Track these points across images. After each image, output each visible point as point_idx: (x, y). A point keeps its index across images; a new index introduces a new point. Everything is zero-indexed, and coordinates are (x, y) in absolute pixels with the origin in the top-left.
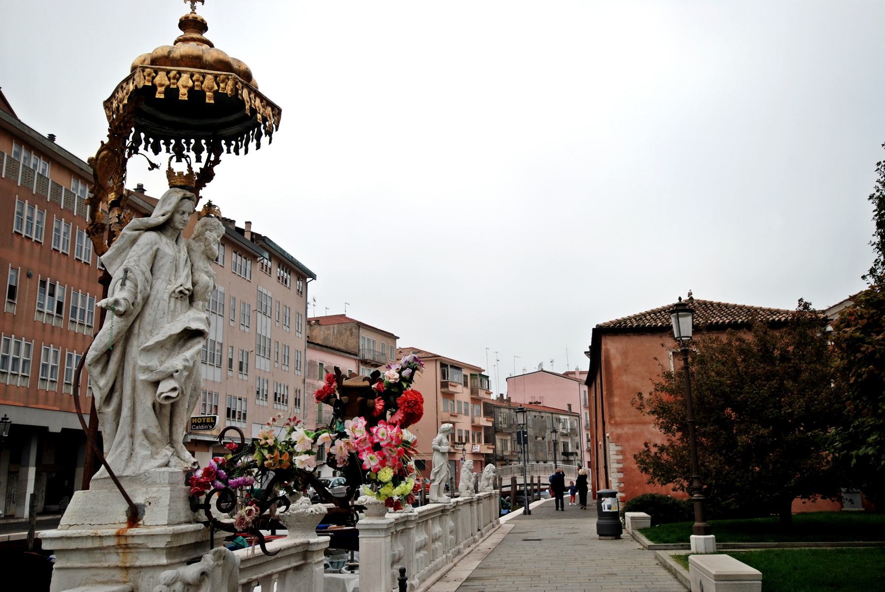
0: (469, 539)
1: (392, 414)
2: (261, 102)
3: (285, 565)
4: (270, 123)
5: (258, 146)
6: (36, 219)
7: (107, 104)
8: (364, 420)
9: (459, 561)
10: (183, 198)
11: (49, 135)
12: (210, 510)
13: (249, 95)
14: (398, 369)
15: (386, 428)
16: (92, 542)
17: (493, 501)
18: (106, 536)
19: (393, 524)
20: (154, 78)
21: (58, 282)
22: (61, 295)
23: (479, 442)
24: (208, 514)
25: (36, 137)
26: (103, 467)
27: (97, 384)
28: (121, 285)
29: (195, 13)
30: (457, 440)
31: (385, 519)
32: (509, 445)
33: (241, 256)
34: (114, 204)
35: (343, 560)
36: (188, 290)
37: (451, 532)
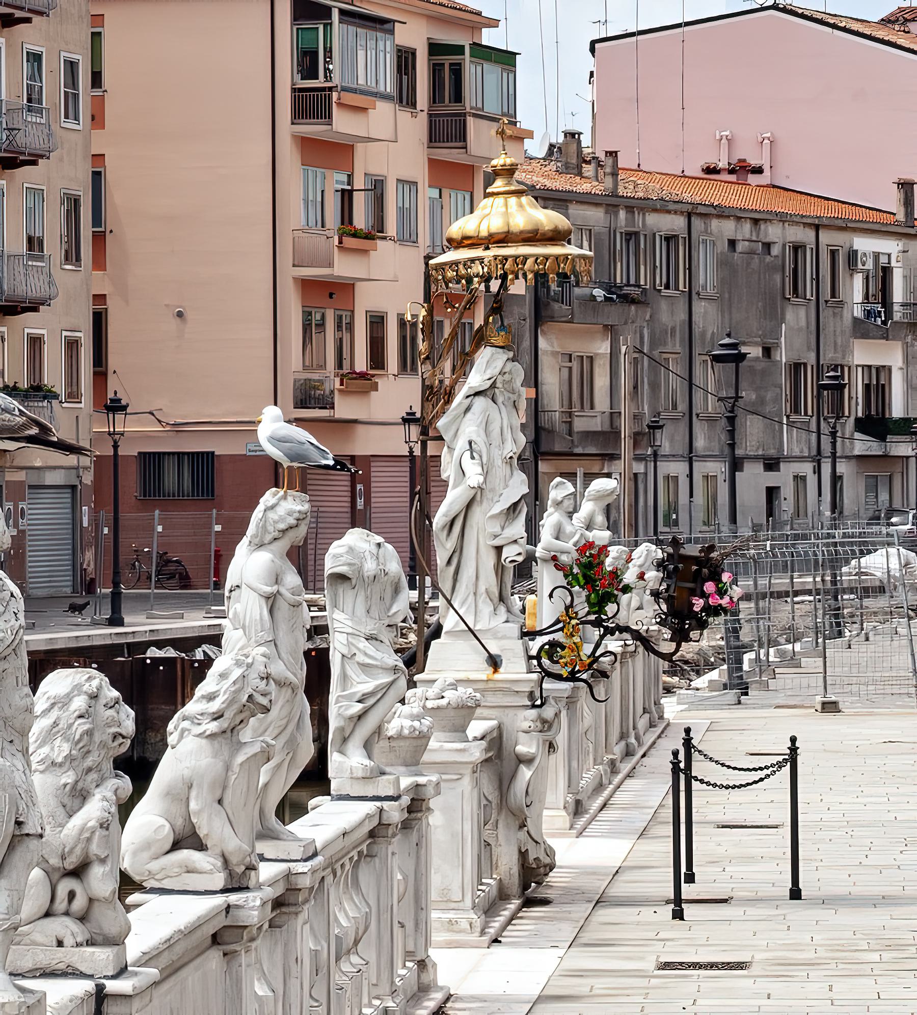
9: (504, 928)
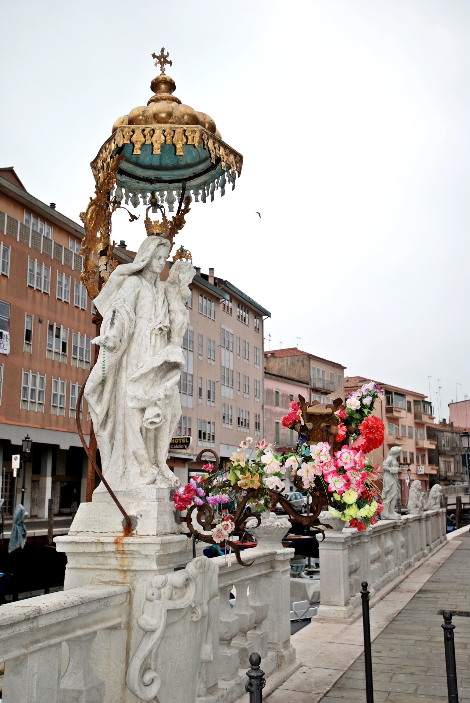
0: (418, 554)
1: (355, 440)
2: (225, 150)
3: (256, 572)
4: (233, 170)
5: (223, 194)
6: (43, 274)
7: (94, 164)
8: (328, 444)
9: (411, 573)
10: (159, 245)
11: (51, 204)
12: (192, 523)
13: (214, 145)
14: (359, 396)
15: (350, 453)
16: (96, 547)
17: (440, 518)
18: (107, 543)
19: (350, 539)
20: (132, 136)
21: (62, 326)
22: (64, 337)
23: (423, 463)
24: (190, 526)
25: (41, 206)
26: (102, 482)
27: (94, 411)
28: (111, 324)
29: (165, 74)
30: (402, 461)
31: (342, 533)
32: (452, 466)
33: (206, 298)
34: (103, 253)
35: (301, 565)
36: (166, 327)
37: (402, 547)
